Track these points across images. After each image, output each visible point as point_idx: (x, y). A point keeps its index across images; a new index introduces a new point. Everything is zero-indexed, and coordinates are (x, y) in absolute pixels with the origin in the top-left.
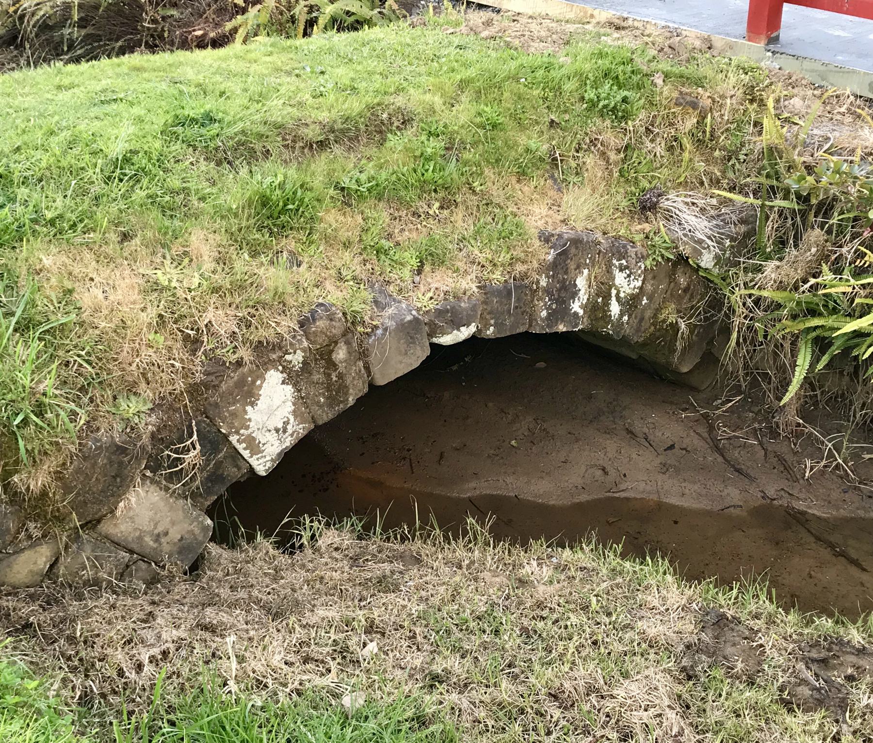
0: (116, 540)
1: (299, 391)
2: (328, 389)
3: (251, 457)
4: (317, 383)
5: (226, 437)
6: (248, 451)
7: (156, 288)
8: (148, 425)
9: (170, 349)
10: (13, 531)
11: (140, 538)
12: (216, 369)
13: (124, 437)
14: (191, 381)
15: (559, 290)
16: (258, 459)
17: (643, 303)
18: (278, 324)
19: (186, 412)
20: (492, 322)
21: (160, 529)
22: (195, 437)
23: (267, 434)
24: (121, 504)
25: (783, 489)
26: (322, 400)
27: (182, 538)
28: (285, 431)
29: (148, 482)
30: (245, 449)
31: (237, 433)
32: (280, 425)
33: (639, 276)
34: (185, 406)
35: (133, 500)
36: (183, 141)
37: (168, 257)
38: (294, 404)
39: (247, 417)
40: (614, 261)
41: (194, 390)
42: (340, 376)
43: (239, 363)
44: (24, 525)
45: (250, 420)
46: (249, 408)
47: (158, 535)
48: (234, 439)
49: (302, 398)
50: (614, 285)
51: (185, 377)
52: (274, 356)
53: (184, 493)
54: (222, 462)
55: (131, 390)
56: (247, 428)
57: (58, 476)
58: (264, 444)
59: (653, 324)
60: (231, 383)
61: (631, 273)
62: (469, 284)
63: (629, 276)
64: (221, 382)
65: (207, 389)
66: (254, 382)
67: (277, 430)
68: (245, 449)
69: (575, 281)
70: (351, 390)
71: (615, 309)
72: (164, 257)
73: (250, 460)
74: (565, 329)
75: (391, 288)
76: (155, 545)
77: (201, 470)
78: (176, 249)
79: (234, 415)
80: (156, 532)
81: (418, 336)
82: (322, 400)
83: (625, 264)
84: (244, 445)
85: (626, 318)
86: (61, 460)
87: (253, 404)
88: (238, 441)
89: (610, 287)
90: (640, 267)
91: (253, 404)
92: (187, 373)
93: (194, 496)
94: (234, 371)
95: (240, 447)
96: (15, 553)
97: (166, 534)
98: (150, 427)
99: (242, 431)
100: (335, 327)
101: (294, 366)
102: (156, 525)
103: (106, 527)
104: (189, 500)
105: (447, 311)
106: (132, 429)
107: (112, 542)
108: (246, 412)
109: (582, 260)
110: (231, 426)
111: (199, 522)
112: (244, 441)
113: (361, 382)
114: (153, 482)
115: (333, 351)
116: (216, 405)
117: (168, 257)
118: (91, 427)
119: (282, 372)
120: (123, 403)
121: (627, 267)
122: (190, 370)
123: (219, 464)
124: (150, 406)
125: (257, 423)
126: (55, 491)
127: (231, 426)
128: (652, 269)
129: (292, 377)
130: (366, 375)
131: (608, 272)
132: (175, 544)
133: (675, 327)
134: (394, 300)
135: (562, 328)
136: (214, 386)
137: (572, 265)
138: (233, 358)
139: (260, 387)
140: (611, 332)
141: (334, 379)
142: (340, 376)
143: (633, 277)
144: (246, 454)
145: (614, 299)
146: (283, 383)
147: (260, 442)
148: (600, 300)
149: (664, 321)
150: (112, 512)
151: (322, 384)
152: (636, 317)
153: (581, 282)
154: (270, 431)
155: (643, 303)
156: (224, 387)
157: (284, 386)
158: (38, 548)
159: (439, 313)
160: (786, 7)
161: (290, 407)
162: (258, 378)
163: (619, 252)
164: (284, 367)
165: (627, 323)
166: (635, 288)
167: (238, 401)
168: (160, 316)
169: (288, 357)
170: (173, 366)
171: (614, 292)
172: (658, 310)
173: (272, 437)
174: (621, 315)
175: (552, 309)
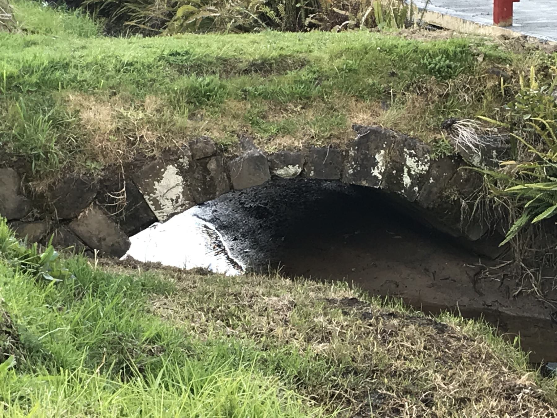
0: (78, 234)
1: (187, 181)
2: (204, 184)
3: (155, 210)
4: (197, 179)
5: (142, 196)
6: (154, 207)
7: (120, 117)
8: (99, 175)
9: (119, 144)
10: (26, 211)
11: (90, 238)
12: (141, 157)
13: (85, 177)
14: (126, 161)
15: (362, 160)
16: (159, 213)
17: (431, 182)
18: (177, 142)
19: (121, 176)
20: (313, 168)
21: (101, 236)
22: (124, 189)
23: (166, 200)
24: (81, 214)
25: (497, 301)
26: (200, 189)
27: (113, 245)
28: (177, 202)
29: (97, 207)
30: (152, 205)
31: (148, 195)
32: (174, 198)
33: (426, 163)
34: (121, 173)
35: (87, 212)
36: (166, 61)
37: (133, 106)
38: (183, 188)
39: (155, 187)
40: (405, 150)
41: (127, 166)
42: (212, 178)
43: (153, 158)
44: (32, 210)
45: (156, 189)
46: (156, 183)
47: (100, 238)
48: (146, 197)
49: (189, 186)
50: (405, 164)
51: (124, 159)
52: (172, 158)
53: (116, 219)
54: (139, 209)
55: (94, 158)
56: (154, 194)
57: (50, 187)
58: (163, 206)
59: (439, 197)
60: (147, 167)
61: (419, 160)
62: (299, 144)
63: (417, 161)
64: (142, 165)
65: (134, 168)
66: (160, 169)
67: (172, 200)
68: (152, 205)
69: (374, 156)
70: (218, 189)
71: (407, 180)
72: (131, 105)
73: (155, 212)
74: (367, 185)
75: (255, 141)
76: (98, 244)
77: (127, 209)
78: (137, 103)
79: (148, 184)
80: (99, 236)
81: (263, 167)
82: (200, 189)
83: (414, 153)
84: (152, 202)
85: (416, 188)
86: (52, 180)
87: (159, 181)
88: (149, 199)
89: (403, 166)
90: (426, 158)
91: (159, 181)
92: (124, 157)
93: (122, 223)
94: (150, 161)
95: (150, 203)
96: (26, 222)
97: (104, 239)
98: (99, 176)
99: (151, 195)
100: (208, 149)
101: (184, 166)
102: (100, 232)
103: (72, 225)
104: (119, 225)
105: (282, 155)
106: (90, 174)
107: (76, 235)
108: (154, 185)
109: (380, 144)
110: (145, 190)
111: (123, 239)
112: (151, 200)
113: (224, 184)
114: (101, 209)
115: (208, 163)
116: (138, 177)
117: (133, 106)
118: (70, 168)
119: (177, 168)
120: (89, 163)
121: (415, 156)
122: (127, 156)
123: (137, 210)
124: (103, 168)
125: (160, 192)
126: (48, 194)
127: (145, 190)
128: (435, 160)
129: (181, 171)
130: (228, 182)
131: (400, 155)
132: (109, 247)
133: (457, 203)
134: (255, 147)
135: (364, 183)
136: (138, 167)
137: (372, 146)
138: (150, 154)
139: (163, 173)
140: (405, 196)
141: (208, 179)
142: (212, 178)
143: (420, 163)
144: (153, 208)
145: (406, 174)
146: (177, 174)
147: (161, 204)
148: (394, 172)
149: (448, 197)
150: (77, 217)
151: (201, 180)
152: (425, 190)
153: (379, 158)
154: (168, 199)
155: (431, 182)
156: (144, 168)
157: (177, 176)
158: (37, 224)
159: (278, 156)
160: (514, 3)
161: (180, 189)
162: (163, 168)
163: (409, 145)
164: (178, 165)
165: (418, 192)
166: (422, 170)
167: (151, 177)
168: (118, 129)
169: (181, 160)
170: (119, 152)
171: (406, 170)
172: (442, 190)
173: (169, 203)
174: (412, 185)
175: (357, 170)
